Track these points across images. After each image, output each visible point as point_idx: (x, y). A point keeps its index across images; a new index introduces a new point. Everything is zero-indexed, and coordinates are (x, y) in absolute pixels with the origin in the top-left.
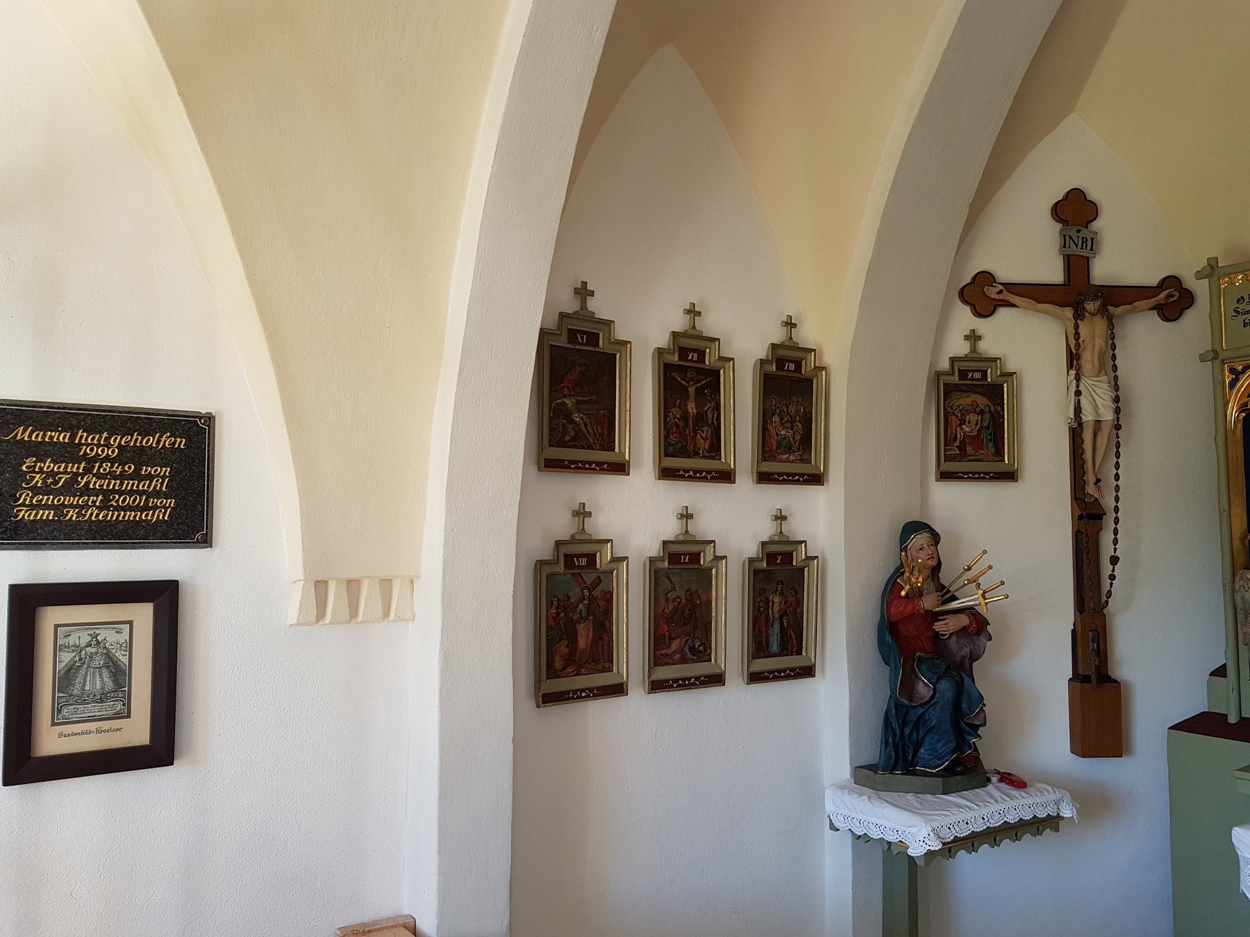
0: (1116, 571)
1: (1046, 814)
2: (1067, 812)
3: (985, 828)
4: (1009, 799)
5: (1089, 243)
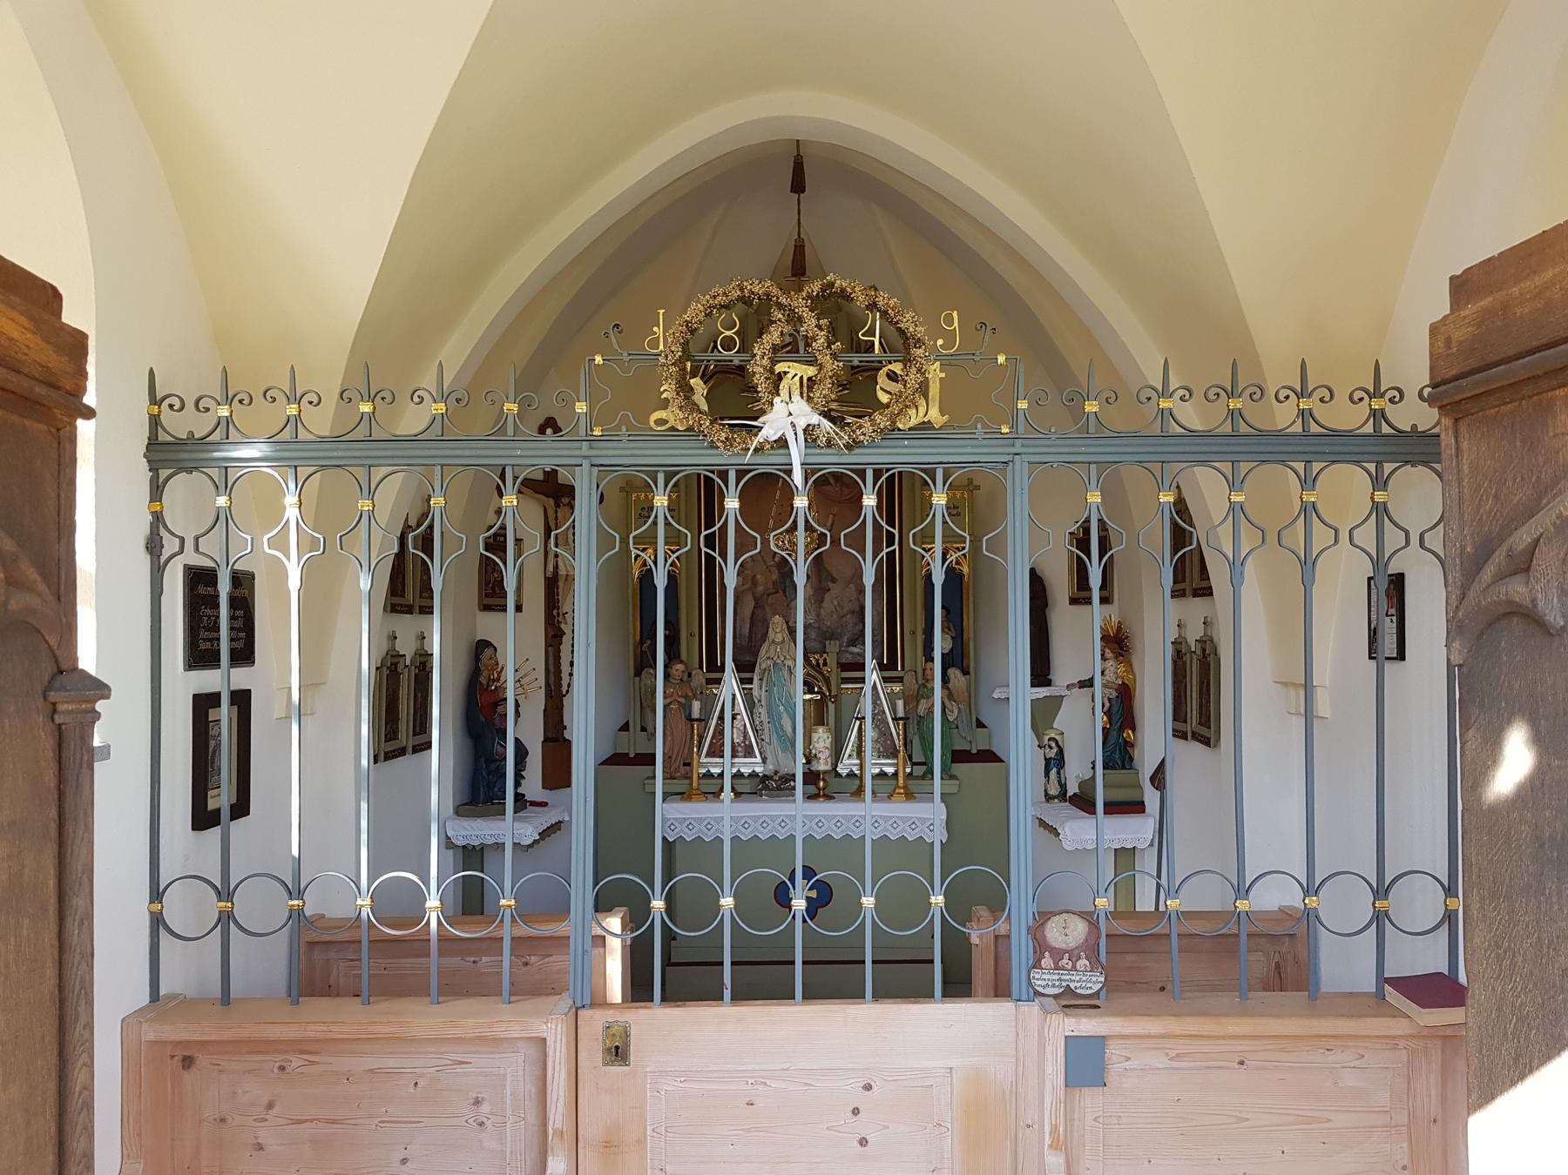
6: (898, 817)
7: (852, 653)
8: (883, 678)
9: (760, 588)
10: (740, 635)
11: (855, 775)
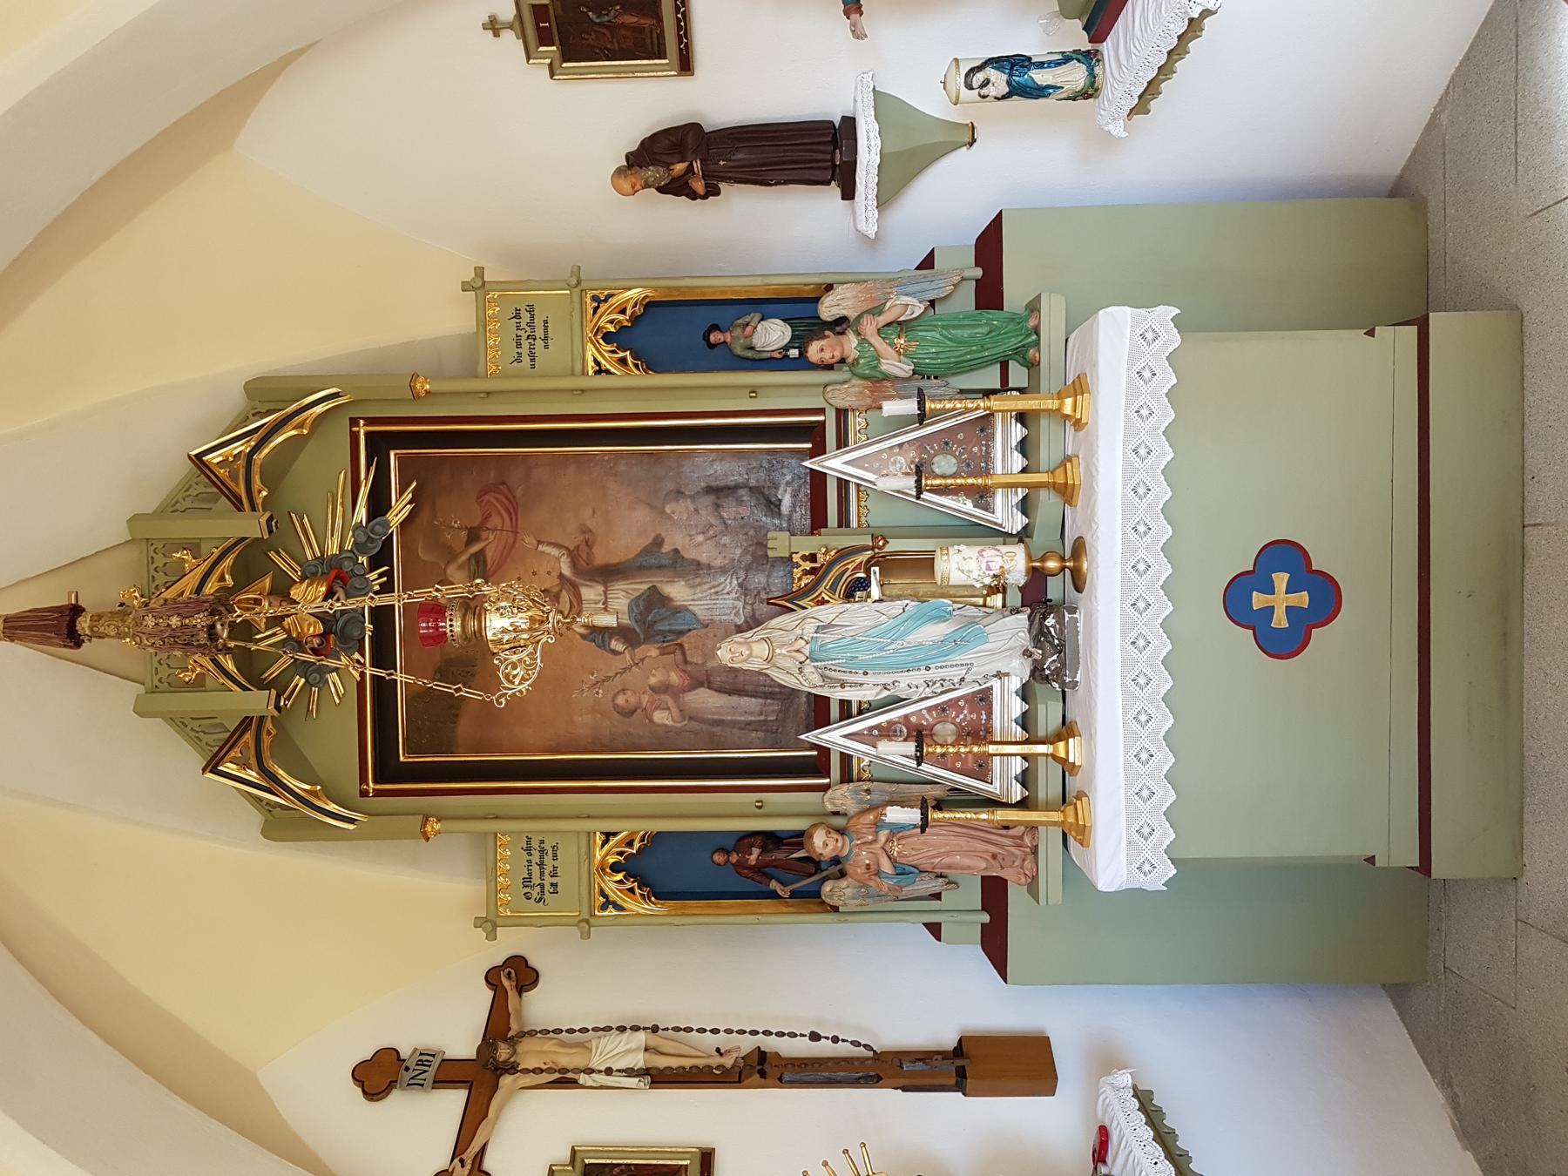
0: (827, 1035)
1: (1133, 1099)
2: (1125, 1079)
3: (1167, 1162)
4: (1124, 1139)
5: (424, 1058)
6: (1127, 406)
7: (794, 505)
8: (839, 447)
9: (675, 678)
10: (761, 714)
11: (1025, 498)
